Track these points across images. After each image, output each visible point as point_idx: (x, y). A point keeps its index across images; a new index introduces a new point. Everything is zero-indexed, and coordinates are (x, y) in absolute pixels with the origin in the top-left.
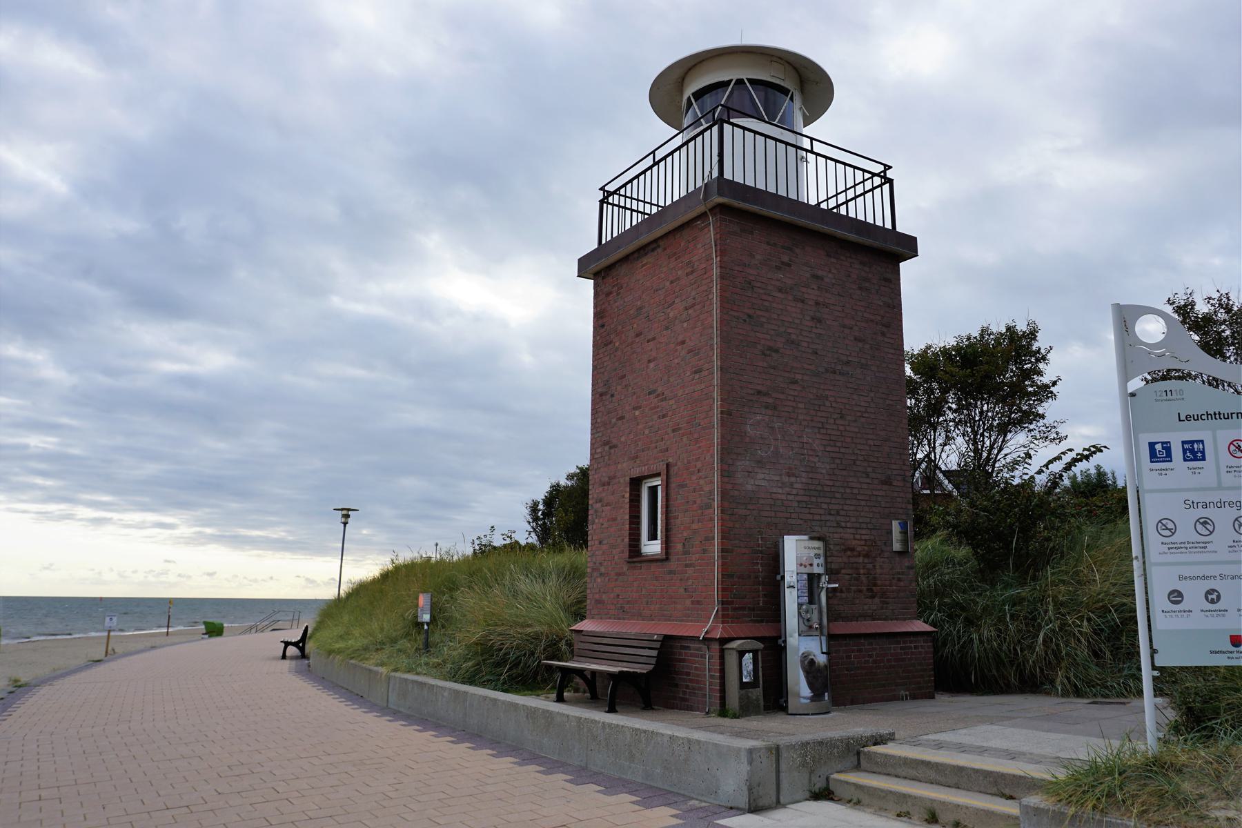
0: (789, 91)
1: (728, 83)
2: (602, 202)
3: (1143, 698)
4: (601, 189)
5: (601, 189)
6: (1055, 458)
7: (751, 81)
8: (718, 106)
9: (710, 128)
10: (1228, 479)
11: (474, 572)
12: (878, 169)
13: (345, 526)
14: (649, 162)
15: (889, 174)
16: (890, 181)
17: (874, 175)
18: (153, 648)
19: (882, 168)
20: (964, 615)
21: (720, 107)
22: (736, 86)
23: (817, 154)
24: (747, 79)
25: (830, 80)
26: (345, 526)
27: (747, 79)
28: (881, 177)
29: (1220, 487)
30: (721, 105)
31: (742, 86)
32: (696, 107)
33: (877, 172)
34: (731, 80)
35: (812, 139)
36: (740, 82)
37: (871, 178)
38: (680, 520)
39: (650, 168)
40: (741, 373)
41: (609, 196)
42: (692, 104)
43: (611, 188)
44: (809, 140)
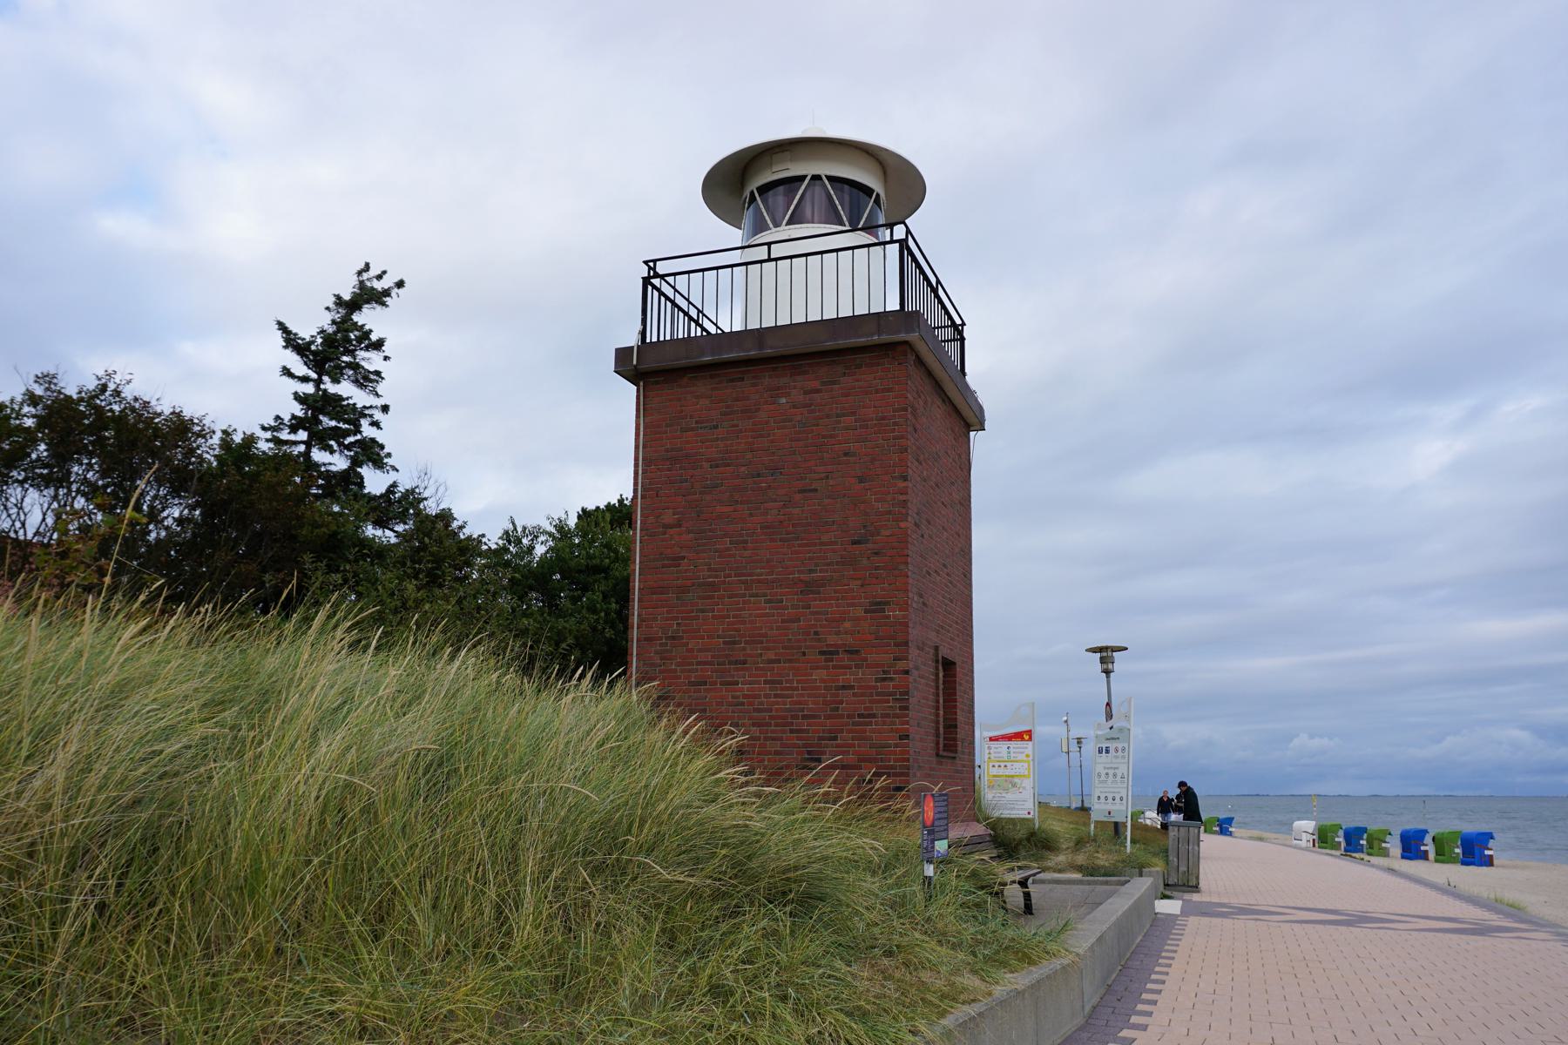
0: (873, 191)
1: (802, 178)
2: (646, 281)
4: (646, 263)
5: (646, 263)
6: (286, 328)
10: (1114, 760)
11: (923, 643)
13: (1108, 677)
18: (1261, 839)
20: (743, 640)
22: (813, 182)
25: (922, 177)
26: (1108, 677)
29: (1112, 763)
31: (818, 182)
32: (760, 202)
34: (805, 177)
36: (816, 178)
39: (761, 262)
42: (755, 199)
43: (662, 268)
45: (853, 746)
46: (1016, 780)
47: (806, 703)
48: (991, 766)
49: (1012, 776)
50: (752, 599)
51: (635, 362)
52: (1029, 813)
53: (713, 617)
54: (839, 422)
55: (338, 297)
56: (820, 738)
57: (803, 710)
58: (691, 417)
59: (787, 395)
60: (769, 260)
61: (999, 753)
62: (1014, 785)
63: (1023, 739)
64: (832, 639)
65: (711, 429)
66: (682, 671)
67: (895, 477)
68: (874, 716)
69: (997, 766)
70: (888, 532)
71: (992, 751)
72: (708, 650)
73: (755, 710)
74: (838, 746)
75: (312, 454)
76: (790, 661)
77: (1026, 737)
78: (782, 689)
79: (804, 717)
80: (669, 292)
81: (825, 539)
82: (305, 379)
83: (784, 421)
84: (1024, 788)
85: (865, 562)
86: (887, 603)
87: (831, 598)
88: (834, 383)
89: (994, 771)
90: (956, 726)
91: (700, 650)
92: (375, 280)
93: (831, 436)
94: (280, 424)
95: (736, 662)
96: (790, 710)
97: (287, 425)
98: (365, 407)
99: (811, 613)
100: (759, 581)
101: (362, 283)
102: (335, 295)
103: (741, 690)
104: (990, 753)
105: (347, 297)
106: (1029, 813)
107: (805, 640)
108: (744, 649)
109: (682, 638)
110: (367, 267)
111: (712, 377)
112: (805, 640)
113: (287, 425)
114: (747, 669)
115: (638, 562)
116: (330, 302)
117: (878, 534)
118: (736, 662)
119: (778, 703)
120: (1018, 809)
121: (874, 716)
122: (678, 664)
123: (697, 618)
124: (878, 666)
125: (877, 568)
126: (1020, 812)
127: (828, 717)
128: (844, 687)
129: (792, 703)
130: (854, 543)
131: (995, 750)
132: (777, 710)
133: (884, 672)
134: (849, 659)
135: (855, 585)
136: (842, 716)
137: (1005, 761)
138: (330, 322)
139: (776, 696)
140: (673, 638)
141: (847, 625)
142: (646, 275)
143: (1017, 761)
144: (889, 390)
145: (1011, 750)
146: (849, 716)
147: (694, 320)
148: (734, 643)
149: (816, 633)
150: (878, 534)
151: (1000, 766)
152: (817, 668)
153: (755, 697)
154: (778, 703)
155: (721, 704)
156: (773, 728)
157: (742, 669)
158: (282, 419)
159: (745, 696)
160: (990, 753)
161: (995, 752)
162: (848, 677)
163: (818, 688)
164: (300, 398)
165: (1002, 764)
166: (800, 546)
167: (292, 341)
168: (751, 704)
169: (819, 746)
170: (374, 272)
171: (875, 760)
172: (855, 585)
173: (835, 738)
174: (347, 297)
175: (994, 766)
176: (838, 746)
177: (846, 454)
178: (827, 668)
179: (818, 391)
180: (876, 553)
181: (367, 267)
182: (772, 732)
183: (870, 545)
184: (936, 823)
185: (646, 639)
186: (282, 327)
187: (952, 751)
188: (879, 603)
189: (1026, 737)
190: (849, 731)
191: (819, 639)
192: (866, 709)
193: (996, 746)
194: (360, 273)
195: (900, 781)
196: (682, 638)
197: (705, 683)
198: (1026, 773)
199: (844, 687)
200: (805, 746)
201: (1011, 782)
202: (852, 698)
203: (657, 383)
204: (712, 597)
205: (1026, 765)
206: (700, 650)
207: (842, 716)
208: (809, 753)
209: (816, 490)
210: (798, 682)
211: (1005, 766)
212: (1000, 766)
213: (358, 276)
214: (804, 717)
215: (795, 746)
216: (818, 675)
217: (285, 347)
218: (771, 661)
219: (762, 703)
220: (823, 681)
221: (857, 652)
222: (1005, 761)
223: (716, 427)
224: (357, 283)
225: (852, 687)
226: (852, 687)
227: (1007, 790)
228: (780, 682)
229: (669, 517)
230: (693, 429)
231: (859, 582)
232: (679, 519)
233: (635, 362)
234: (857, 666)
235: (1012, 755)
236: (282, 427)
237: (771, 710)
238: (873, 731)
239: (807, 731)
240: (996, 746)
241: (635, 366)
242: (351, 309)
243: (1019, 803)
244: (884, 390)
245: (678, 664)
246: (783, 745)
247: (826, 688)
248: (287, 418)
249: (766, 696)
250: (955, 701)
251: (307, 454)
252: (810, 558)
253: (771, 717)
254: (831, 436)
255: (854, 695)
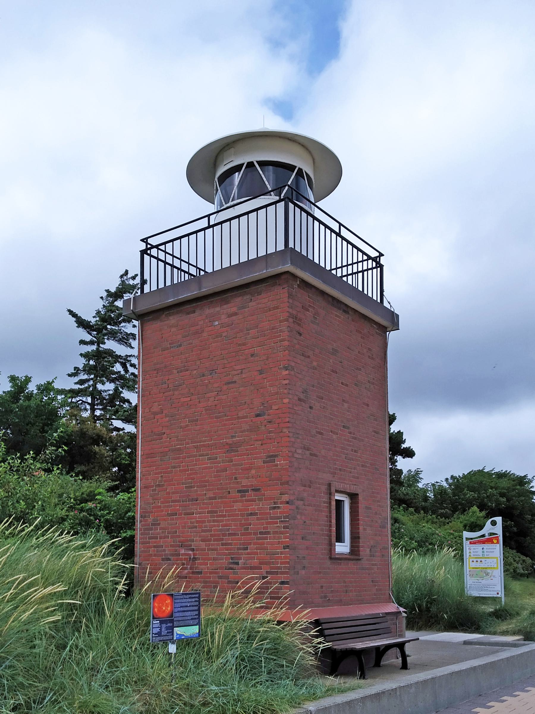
2: (143, 253)
3: (319, 619)
4: (142, 240)
5: (142, 240)
7: (262, 164)
8: (286, 186)
9: (275, 203)
12: (374, 254)
14: (204, 223)
15: (383, 261)
16: (381, 267)
17: (369, 258)
19: (378, 254)
21: (287, 188)
23: (343, 238)
24: (257, 162)
27: (257, 162)
28: (376, 261)
30: (288, 186)
33: (373, 256)
34: (243, 164)
35: (340, 225)
36: (250, 165)
37: (367, 260)
38: (364, 531)
39: (204, 229)
40: (290, 409)
41: (150, 249)
43: (153, 241)
44: (338, 224)
45: (256, 553)
46: (489, 571)
47: (229, 525)
48: (471, 561)
49: (486, 568)
50: (201, 457)
51: (132, 308)
52: (498, 594)
53: (180, 471)
54: (248, 334)
55: (107, 291)
56: (239, 549)
57: (228, 530)
58: (167, 341)
59: (219, 319)
60: (209, 227)
61: (477, 552)
62: (487, 574)
63: (493, 543)
64: (245, 482)
65: (177, 347)
66: (165, 507)
67: (281, 368)
68: (268, 533)
69: (479, 561)
70: (276, 407)
71: (471, 551)
72: (177, 493)
73: (203, 531)
74: (248, 554)
75: (97, 385)
76: (221, 498)
77: (495, 541)
78: (217, 516)
79: (230, 535)
80: (162, 256)
81: (240, 415)
82: (92, 343)
83: (217, 337)
84: (494, 576)
85: (263, 428)
86: (276, 456)
87: (244, 454)
88: (244, 307)
89: (474, 565)
90: (359, 538)
91: (173, 493)
92: (131, 279)
93: (244, 344)
94: (77, 371)
95: (192, 500)
96: (221, 530)
97: (81, 371)
98: (127, 356)
99: (234, 465)
100: (204, 446)
101: (123, 282)
102: (106, 290)
103: (195, 518)
104: (470, 553)
105: (113, 290)
106: (498, 594)
107: (230, 483)
108: (197, 491)
109: (163, 485)
110: (127, 272)
111: (178, 313)
112: (230, 483)
113: (81, 371)
114: (198, 504)
115: (140, 438)
116: (105, 294)
117: (271, 408)
118: (192, 500)
119: (214, 526)
120: (490, 591)
121: (268, 533)
122: (162, 503)
123: (171, 472)
124: (271, 499)
125: (270, 432)
126: (492, 593)
127: (242, 534)
128: (251, 514)
129: (222, 526)
130: (258, 415)
131: (474, 551)
132: (215, 530)
133: (275, 503)
134: (255, 495)
135: (258, 444)
136: (250, 534)
137: (481, 558)
138: (103, 307)
139: (214, 521)
140: (159, 486)
141: (253, 472)
142: (381, 257)
143: (488, 558)
144: (277, 308)
145: (485, 550)
146: (255, 534)
147: (187, 273)
148: (191, 487)
149: (236, 478)
150: (271, 408)
151: (477, 561)
152: (237, 501)
153: (204, 522)
154: (214, 526)
155: (184, 527)
156: (212, 542)
157: (195, 504)
158: (79, 368)
159: (198, 522)
160: (470, 553)
161: (473, 552)
162: (254, 507)
163: (237, 515)
164: (86, 356)
165: (479, 560)
166: (226, 420)
167: (82, 323)
168: (200, 527)
169: (238, 554)
170: (129, 275)
171: (270, 563)
172: (258, 444)
173: (246, 549)
174: (113, 290)
175: (473, 561)
176: (248, 554)
177: (252, 355)
178: (241, 501)
179: (236, 314)
180: (270, 422)
181: (127, 272)
182: (213, 545)
183: (266, 417)
184: (175, 615)
185: (145, 487)
186: (71, 312)
187: (356, 555)
188: (272, 456)
189: (495, 541)
190: (255, 544)
191: (238, 482)
192: (264, 528)
193: (474, 547)
194: (122, 277)
195: (284, 578)
196: (163, 485)
197: (176, 514)
198: (495, 566)
199: (251, 514)
200: (230, 554)
201: (485, 572)
202: (256, 521)
203: (149, 320)
204: (179, 458)
205: (495, 560)
206: (173, 493)
207: (250, 534)
208: (232, 558)
209: (235, 382)
210: (226, 511)
211: (481, 561)
212: (477, 561)
213: (121, 278)
214: (230, 535)
215: (225, 554)
216: (238, 506)
217: (78, 327)
218: (211, 498)
219: (206, 526)
220: (240, 510)
221: (258, 490)
222: (481, 558)
223: (180, 345)
224: (120, 282)
225: (256, 514)
226: (256, 514)
227: (482, 577)
228: (216, 512)
229: (156, 408)
230: (168, 349)
231: (260, 442)
232: (161, 409)
233: (132, 308)
234: (260, 500)
235: (485, 553)
236: (79, 372)
237: (211, 531)
238: (268, 543)
239: (230, 544)
240: (474, 547)
241: (132, 311)
242: (115, 297)
243: (491, 586)
244: (275, 308)
245: (162, 503)
246: (218, 554)
247: (242, 515)
248: (81, 367)
249: (209, 521)
250: (358, 520)
251: (94, 386)
252: (232, 429)
253: (211, 535)
254: (244, 344)
255: (258, 519)
